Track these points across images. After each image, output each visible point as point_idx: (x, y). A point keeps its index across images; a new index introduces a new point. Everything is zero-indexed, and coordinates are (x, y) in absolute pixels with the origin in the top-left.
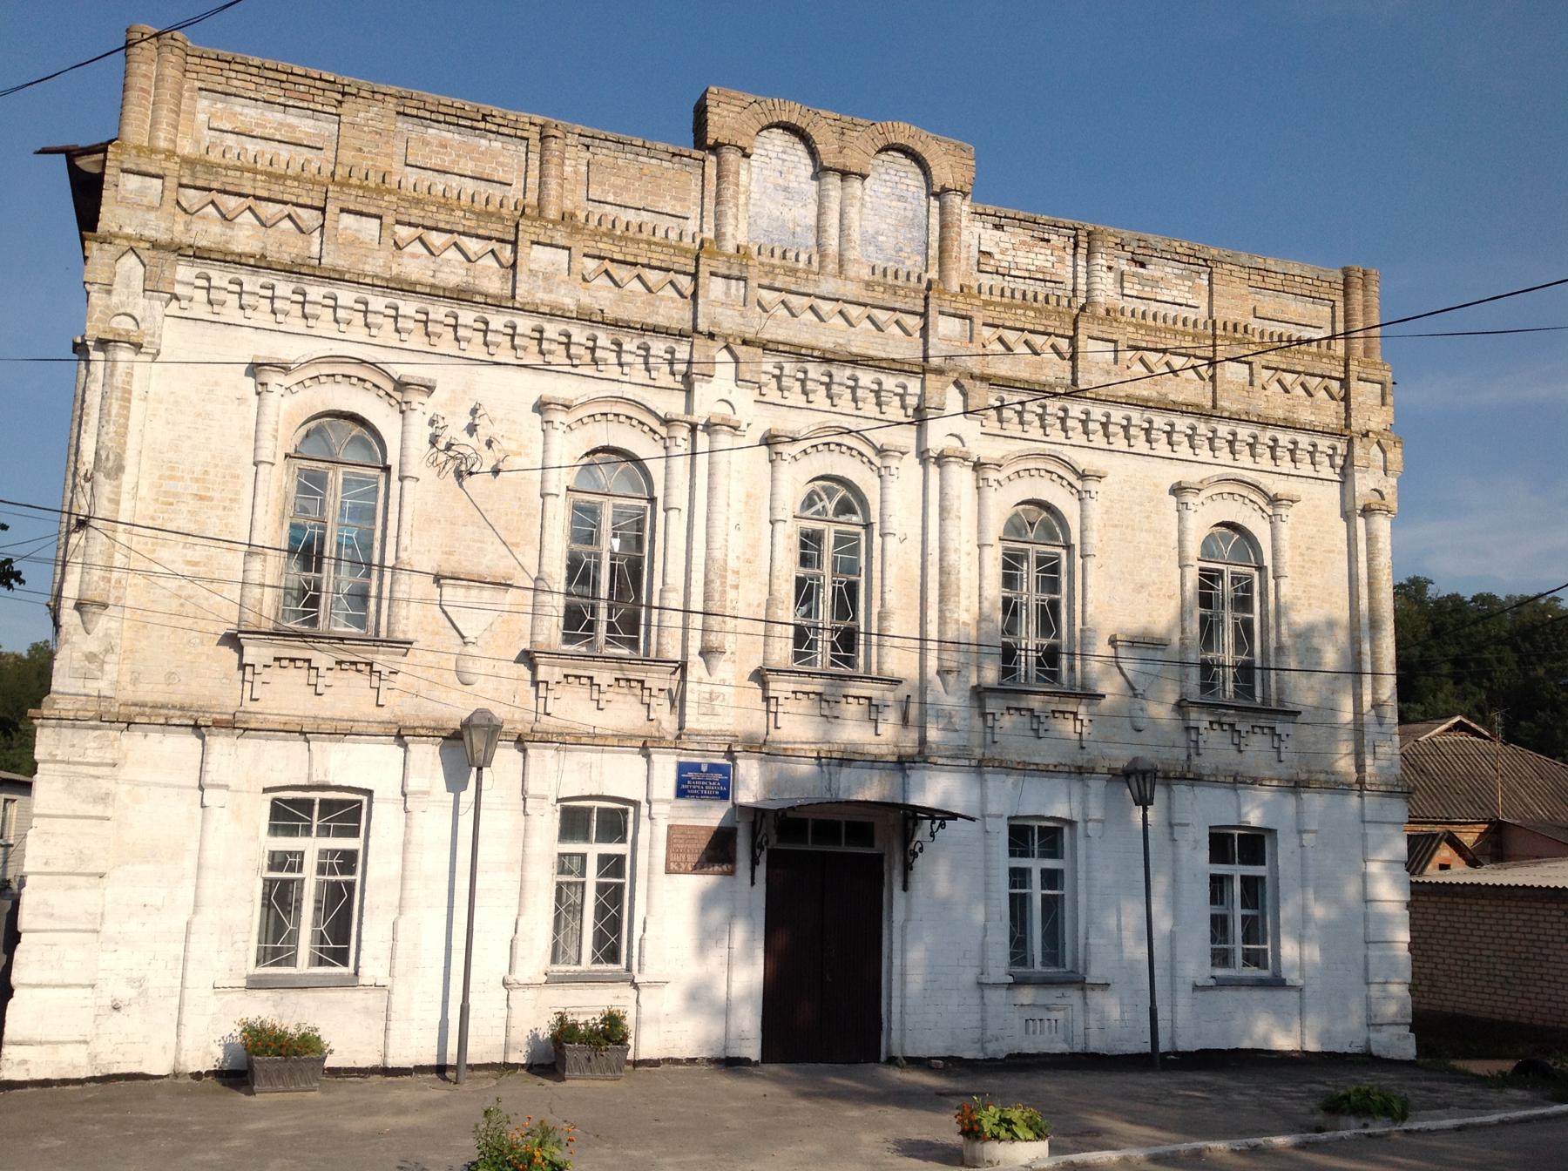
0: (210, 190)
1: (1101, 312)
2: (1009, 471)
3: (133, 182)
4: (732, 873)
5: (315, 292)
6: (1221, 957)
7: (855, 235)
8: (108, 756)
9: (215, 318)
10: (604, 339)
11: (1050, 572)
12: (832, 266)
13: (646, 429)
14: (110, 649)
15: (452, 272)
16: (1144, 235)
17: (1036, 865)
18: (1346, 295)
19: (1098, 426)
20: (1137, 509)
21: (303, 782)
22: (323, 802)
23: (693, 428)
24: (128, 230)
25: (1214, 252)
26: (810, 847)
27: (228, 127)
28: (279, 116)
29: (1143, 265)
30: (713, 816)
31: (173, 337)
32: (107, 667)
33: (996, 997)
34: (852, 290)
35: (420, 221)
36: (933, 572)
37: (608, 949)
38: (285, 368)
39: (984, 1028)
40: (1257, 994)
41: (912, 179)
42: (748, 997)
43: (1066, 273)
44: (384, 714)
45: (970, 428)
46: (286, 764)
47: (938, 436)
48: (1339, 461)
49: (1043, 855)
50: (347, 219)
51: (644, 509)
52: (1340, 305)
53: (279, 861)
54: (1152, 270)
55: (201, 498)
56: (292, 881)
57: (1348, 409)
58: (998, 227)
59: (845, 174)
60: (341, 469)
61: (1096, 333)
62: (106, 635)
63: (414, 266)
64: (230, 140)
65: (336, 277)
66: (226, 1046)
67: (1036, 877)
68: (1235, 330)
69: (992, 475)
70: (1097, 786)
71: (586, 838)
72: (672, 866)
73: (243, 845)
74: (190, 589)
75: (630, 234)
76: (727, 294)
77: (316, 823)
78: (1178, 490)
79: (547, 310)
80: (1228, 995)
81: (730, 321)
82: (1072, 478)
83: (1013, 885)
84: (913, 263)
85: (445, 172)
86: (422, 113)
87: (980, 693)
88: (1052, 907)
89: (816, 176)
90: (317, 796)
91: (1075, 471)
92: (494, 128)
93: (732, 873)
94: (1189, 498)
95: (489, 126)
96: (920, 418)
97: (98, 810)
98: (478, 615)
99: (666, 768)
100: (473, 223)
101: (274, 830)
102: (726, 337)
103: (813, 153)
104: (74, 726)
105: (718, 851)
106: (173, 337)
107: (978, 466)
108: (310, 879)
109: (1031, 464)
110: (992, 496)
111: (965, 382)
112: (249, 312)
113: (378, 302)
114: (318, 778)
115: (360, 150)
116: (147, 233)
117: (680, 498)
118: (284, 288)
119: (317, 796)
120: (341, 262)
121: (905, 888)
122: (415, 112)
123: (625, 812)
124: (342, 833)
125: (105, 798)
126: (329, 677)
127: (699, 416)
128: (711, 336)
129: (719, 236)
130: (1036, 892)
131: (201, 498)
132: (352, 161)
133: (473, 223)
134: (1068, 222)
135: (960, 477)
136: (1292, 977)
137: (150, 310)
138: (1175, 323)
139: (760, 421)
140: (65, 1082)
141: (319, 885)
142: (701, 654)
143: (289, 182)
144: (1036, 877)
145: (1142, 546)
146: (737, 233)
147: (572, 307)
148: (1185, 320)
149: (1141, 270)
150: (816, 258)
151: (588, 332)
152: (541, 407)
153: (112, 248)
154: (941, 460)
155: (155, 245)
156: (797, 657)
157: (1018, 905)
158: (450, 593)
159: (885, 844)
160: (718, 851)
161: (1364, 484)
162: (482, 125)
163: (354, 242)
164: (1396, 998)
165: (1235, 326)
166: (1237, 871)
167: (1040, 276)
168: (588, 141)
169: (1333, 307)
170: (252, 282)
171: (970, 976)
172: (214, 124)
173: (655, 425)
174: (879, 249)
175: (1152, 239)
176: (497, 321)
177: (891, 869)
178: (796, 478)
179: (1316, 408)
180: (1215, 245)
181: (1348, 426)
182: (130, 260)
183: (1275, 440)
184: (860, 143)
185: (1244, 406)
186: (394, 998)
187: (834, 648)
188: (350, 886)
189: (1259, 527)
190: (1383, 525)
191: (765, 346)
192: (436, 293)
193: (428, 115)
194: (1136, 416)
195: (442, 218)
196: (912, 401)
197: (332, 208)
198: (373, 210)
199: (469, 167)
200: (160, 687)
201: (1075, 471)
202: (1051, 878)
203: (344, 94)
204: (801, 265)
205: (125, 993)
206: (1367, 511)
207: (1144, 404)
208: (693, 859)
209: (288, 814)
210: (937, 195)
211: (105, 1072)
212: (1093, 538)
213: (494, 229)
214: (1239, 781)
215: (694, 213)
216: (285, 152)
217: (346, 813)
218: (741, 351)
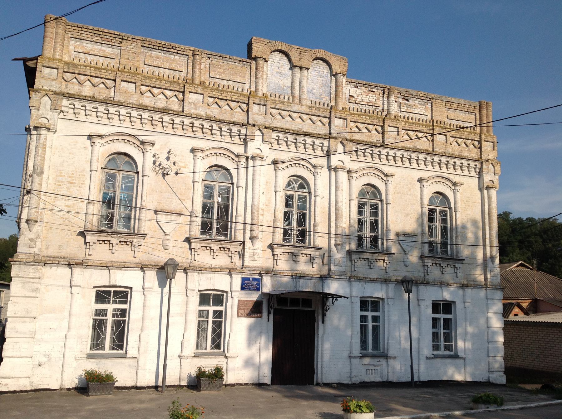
0: (74, 73)
1: (393, 117)
2: (360, 173)
3: (47, 70)
4: (261, 317)
5: (112, 110)
6: (436, 347)
9: (76, 119)
10: (215, 126)
11: (375, 210)
12: (297, 101)
14: (38, 237)
15: (161, 103)
17: (370, 314)
19: (392, 158)
20: (406, 187)
22: (114, 292)
23: (247, 158)
24: (45, 88)
25: (433, 96)
27: (81, 51)
28: (99, 47)
29: (408, 100)
30: (254, 297)
31: (61, 126)
32: (37, 243)
33: (355, 361)
34: (304, 109)
38: (101, 137)
39: (351, 373)
40: (449, 361)
41: (325, 70)
42: (267, 360)
43: (380, 103)
46: (102, 278)
47: (335, 161)
48: (478, 170)
49: (372, 311)
50: (123, 84)
51: (230, 187)
52: (478, 114)
54: (411, 102)
55: (71, 183)
57: (481, 151)
58: (355, 87)
59: (301, 68)
60: (121, 173)
61: (391, 125)
62: (37, 232)
63: (147, 100)
64: (82, 55)
66: (79, 379)
67: (370, 319)
69: (354, 175)
70: (392, 286)
71: (209, 305)
72: (240, 315)
73: (85, 307)
74: (67, 216)
76: (259, 111)
77: (112, 299)
78: (420, 180)
79: (195, 116)
82: (383, 176)
83: (362, 321)
84: (326, 100)
86: (150, 46)
87: (350, 253)
89: (291, 69)
90: (112, 289)
91: (384, 174)
92: (176, 51)
94: (424, 183)
95: (174, 51)
96: (328, 155)
97: (34, 294)
99: (237, 279)
100: (169, 85)
101: (97, 302)
102: (259, 126)
103: (290, 60)
104: (25, 264)
105: (256, 309)
106: (61, 126)
107: (349, 172)
108: (110, 319)
109: (368, 171)
112: (88, 117)
113: (135, 113)
114: (113, 283)
115: (128, 59)
117: (242, 183)
118: (101, 108)
119: (112, 289)
120: (121, 99)
121: (323, 322)
122: (148, 46)
123: (223, 295)
125: (36, 290)
127: (249, 154)
129: (256, 90)
130: (370, 324)
131: (71, 183)
133: (169, 85)
136: (461, 354)
137: (53, 116)
139: (271, 155)
140: (21, 392)
141: (113, 321)
142: (250, 239)
143: (103, 71)
144: (370, 319)
145: (408, 200)
149: (407, 102)
150: (291, 98)
151: (210, 124)
152: (193, 151)
153: (39, 94)
154: (336, 169)
155: (55, 93)
156: (284, 240)
157: (364, 329)
159: (316, 307)
160: (256, 309)
161: (487, 178)
162: (172, 50)
163: (126, 92)
164: (499, 361)
165: (441, 122)
166: (442, 316)
167: (371, 104)
168: (210, 56)
169: (475, 115)
170: (89, 106)
171: (346, 354)
172: (76, 50)
173: (234, 157)
175: (411, 91)
176: (177, 120)
177: (318, 316)
178: (284, 176)
179: (470, 151)
180: (434, 93)
181: (481, 158)
182: (46, 98)
183: (455, 163)
185: (444, 151)
186: (140, 362)
187: (297, 237)
188: (124, 322)
189: (449, 194)
190: (493, 193)
192: (155, 110)
193: (152, 47)
194: (405, 154)
195: (158, 84)
196: (325, 149)
197: (118, 80)
198: (133, 81)
199: (167, 65)
201: (384, 174)
203: (122, 39)
204: (286, 100)
205: (43, 360)
206: (488, 188)
207: (408, 150)
209: (102, 296)
210: (334, 76)
211: (36, 388)
212: (390, 197)
213: (176, 87)
214: (442, 284)
215: (248, 82)
216: (101, 60)
217: (123, 295)
218: (264, 131)
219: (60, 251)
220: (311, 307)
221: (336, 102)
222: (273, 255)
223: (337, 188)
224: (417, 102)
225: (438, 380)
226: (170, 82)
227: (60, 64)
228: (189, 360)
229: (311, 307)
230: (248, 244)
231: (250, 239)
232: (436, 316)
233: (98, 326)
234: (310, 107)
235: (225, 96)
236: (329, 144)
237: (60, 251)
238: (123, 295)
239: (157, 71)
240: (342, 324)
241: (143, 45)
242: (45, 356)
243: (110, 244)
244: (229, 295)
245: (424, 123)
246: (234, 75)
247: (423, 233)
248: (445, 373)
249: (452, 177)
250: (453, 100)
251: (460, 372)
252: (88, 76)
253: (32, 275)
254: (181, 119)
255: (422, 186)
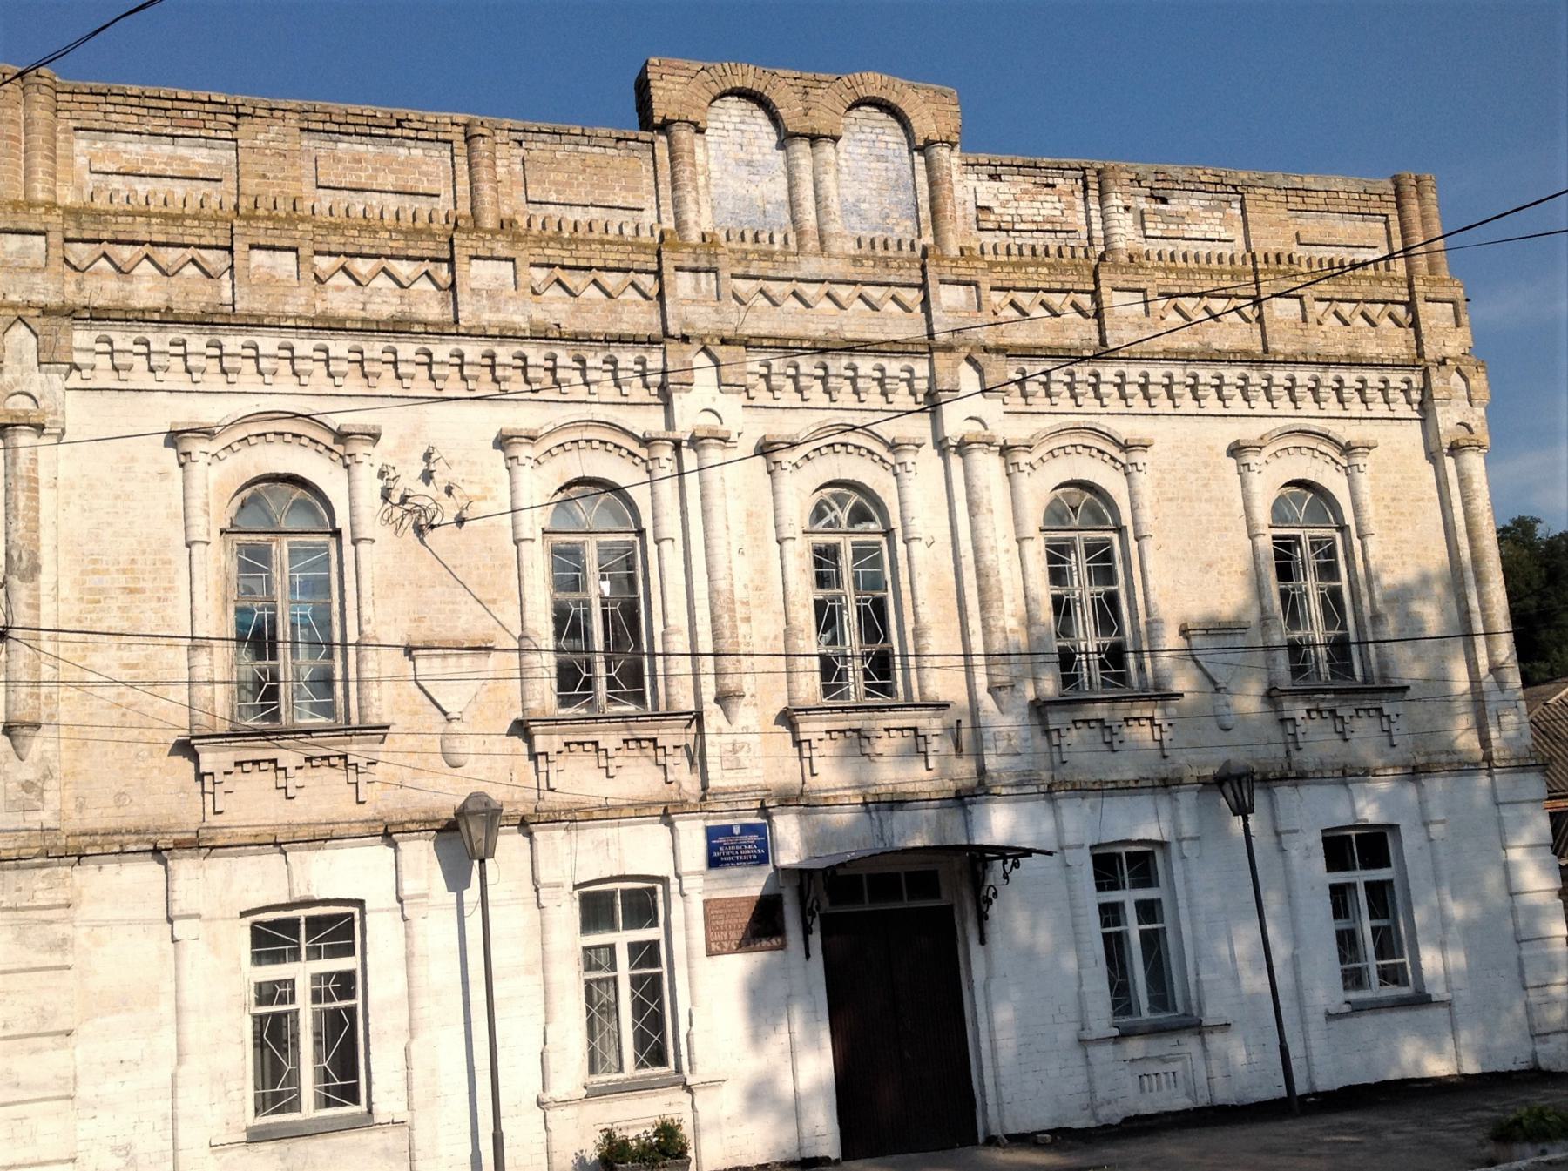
0: (100, 241)
1: (1123, 258)
4: (783, 947)
7: (834, 206)
8: (60, 896)
10: (564, 357)
12: (812, 244)
13: (305, 441)
15: (384, 302)
16: (1161, 167)
17: (1128, 897)
18: (1400, 207)
20: (1192, 477)
21: (284, 900)
22: (309, 920)
23: (677, 446)
25: (1243, 176)
26: (906, 904)
27: (112, 167)
29: (1164, 201)
30: (752, 885)
31: (78, 413)
34: (838, 268)
35: (341, 248)
36: (969, 576)
37: (653, 1049)
38: (208, 433)
40: (1401, 1016)
41: (892, 135)
44: (367, 812)
45: (990, 408)
46: (263, 882)
47: (955, 421)
48: (1416, 396)
50: (259, 257)
51: (633, 544)
53: (267, 993)
54: (1176, 205)
55: (132, 591)
56: (285, 1014)
57: (1418, 336)
60: (286, 540)
61: (1120, 284)
62: (42, 759)
63: (341, 300)
65: (254, 323)
67: (1131, 913)
68: (1279, 261)
70: (1187, 799)
71: (612, 927)
73: (226, 977)
74: (130, 696)
75: (580, 235)
77: (304, 945)
80: (1368, 1022)
81: (704, 319)
82: (1114, 451)
84: (903, 229)
85: (363, 190)
86: (328, 126)
88: (650, 993)
90: (302, 913)
91: (1116, 443)
92: (412, 134)
93: (783, 947)
95: (406, 132)
96: (932, 403)
97: (56, 959)
98: (459, 686)
100: (401, 244)
101: (258, 959)
102: (701, 338)
103: (775, 119)
104: (18, 867)
106: (78, 413)
107: (1006, 450)
108: (305, 1008)
110: (1025, 482)
111: (980, 357)
112: (160, 374)
113: (304, 346)
114: (300, 893)
115: (264, 176)
116: (35, 298)
118: (197, 342)
121: (982, 941)
123: (653, 891)
124: (334, 952)
126: (299, 778)
127: (683, 430)
128: (685, 339)
129: (680, 225)
130: (1133, 929)
132: (256, 191)
133: (401, 244)
134: (1074, 162)
135: (988, 465)
136: (1437, 991)
138: (1209, 261)
139: (749, 427)
142: (717, 700)
144: (1131, 913)
145: (1204, 519)
146: (700, 220)
147: (525, 326)
148: (1220, 257)
149: (1163, 207)
150: (792, 237)
151: (545, 351)
154: (963, 448)
155: (45, 311)
156: (827, 691)
158: (426, 665)
160: (764, 924)
161: (1448, 419)
162: (398, 132)
163: (270, 281)
165: (1278, 257)
166: (1360, 877)
167: (1049, 227)
168: (519, 136)
171: (1067, 1034)
173: (633, 446)
174: (863, 217)
175: (1172, 170)
176: (442, 351)
177: (963, 921)
178: (800, 488)
179: (1382, 339)
180: (1242, 168)
181: (1421, 355)
182: (20, 331)
184: (827, 102)
185: (1300, 346)
190: (1475, 463)
191: (748, 343)
192: (370, 328)
193: (335, 128)
194: (1178, 372)
195: (365, 242)
196: (921, 385)
198: (287, 243)
199: (389, 181)
200: (110, 811)
201: (1116, 443)
202: (646, 954)
204: (777, 247)
206: (1455, 449)
207: (1185, 358)
208: (737, 935)
210: (921, 150)
212: (1146, 516)
213: (426, 247)
214: (1349, 774)
215: (649, 202)
216: (179, 189)
218: (721, 351)
219: (122, 811)
220: (937, 895)
221: (936, 235)
222: (797, 743)
223: (972, 506)
224: (1194, 202)
225: (1371, 1081)
226: (406, 234)
227: (50, 219)
228: (570, 1111)
229: (937, 895)
230: (714, 717)
231: (717, 700)
232: (1341, 877)
233: (273, 1036)
234: (856, 260)
235: (582, 255)
236: (932, 369)
237: (122, 811)
238: (337, 929)
239: (358, 203)
240: (1044, 939)
241: (305, 125)
242: (114, 1149)
243: (277, 769)
244: (674, 888)
245: (1227, 265)
246: (606, 187)
247: (1265, 619)
248: (1393, 1058)
249: (1105, 423)
250: (1309, 181)
251: (1439, 1051)
252: (142, 243)
253: (42, 898)
254: (517, 348)
255: (1244, 470)
